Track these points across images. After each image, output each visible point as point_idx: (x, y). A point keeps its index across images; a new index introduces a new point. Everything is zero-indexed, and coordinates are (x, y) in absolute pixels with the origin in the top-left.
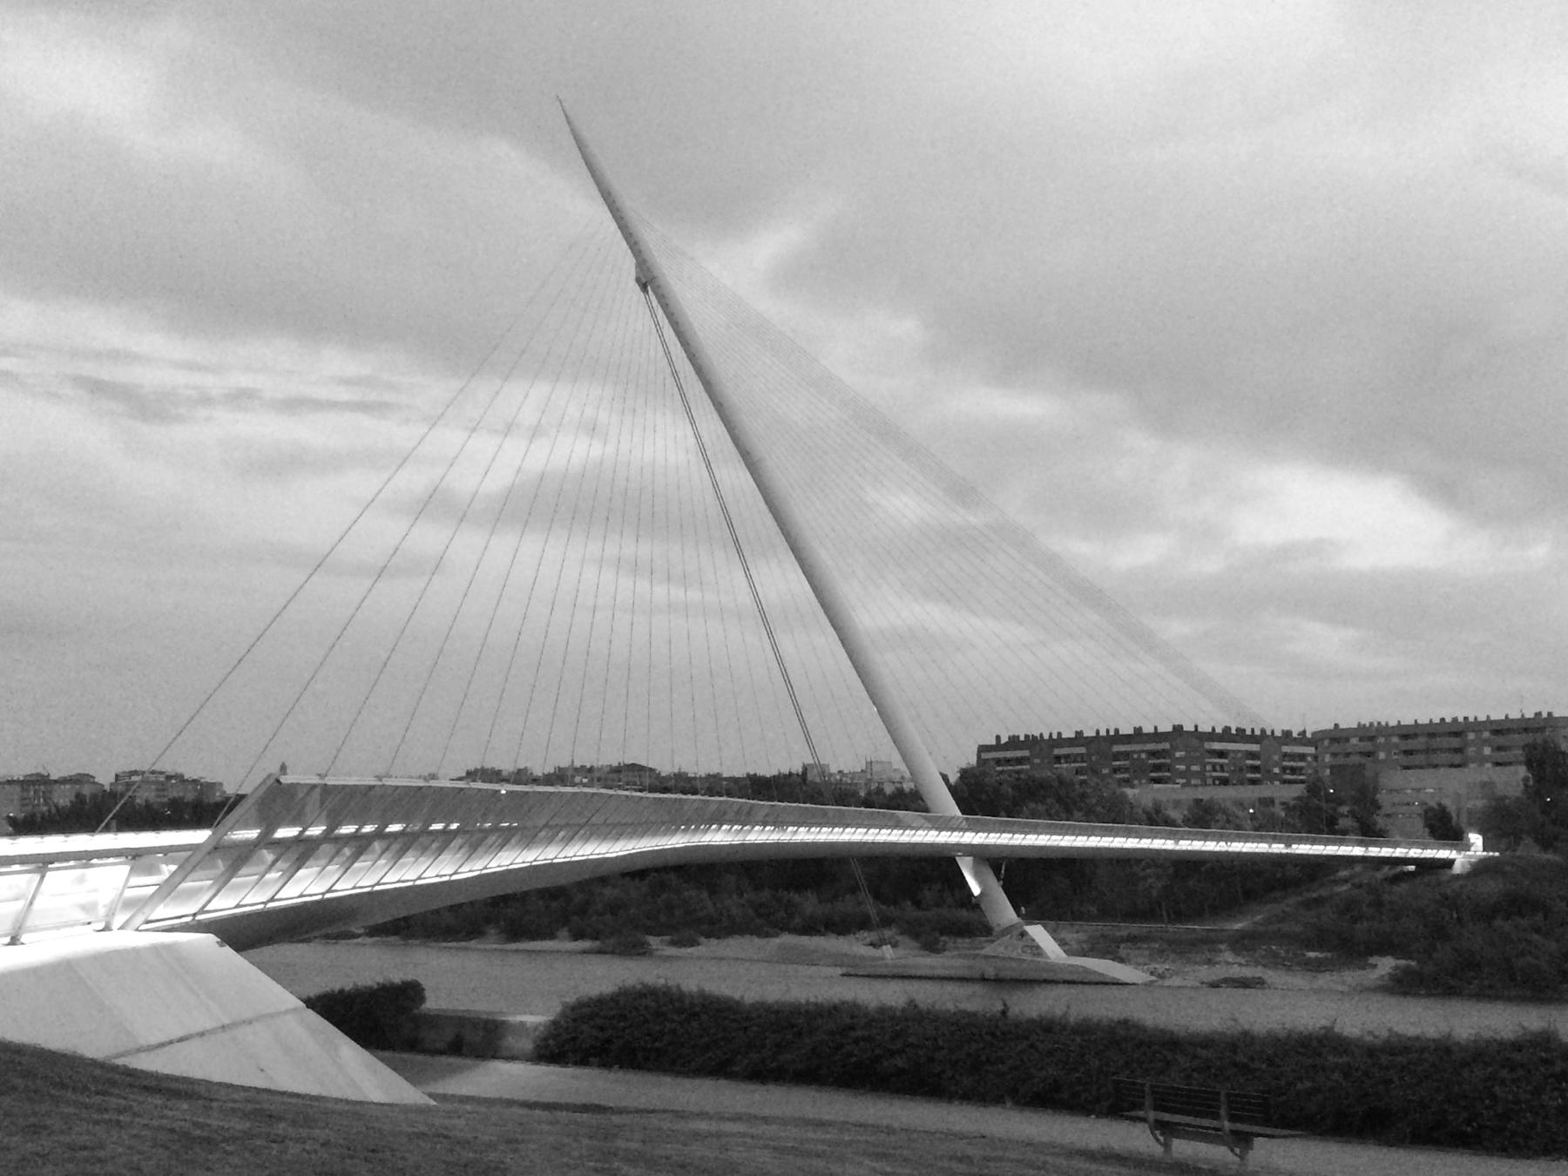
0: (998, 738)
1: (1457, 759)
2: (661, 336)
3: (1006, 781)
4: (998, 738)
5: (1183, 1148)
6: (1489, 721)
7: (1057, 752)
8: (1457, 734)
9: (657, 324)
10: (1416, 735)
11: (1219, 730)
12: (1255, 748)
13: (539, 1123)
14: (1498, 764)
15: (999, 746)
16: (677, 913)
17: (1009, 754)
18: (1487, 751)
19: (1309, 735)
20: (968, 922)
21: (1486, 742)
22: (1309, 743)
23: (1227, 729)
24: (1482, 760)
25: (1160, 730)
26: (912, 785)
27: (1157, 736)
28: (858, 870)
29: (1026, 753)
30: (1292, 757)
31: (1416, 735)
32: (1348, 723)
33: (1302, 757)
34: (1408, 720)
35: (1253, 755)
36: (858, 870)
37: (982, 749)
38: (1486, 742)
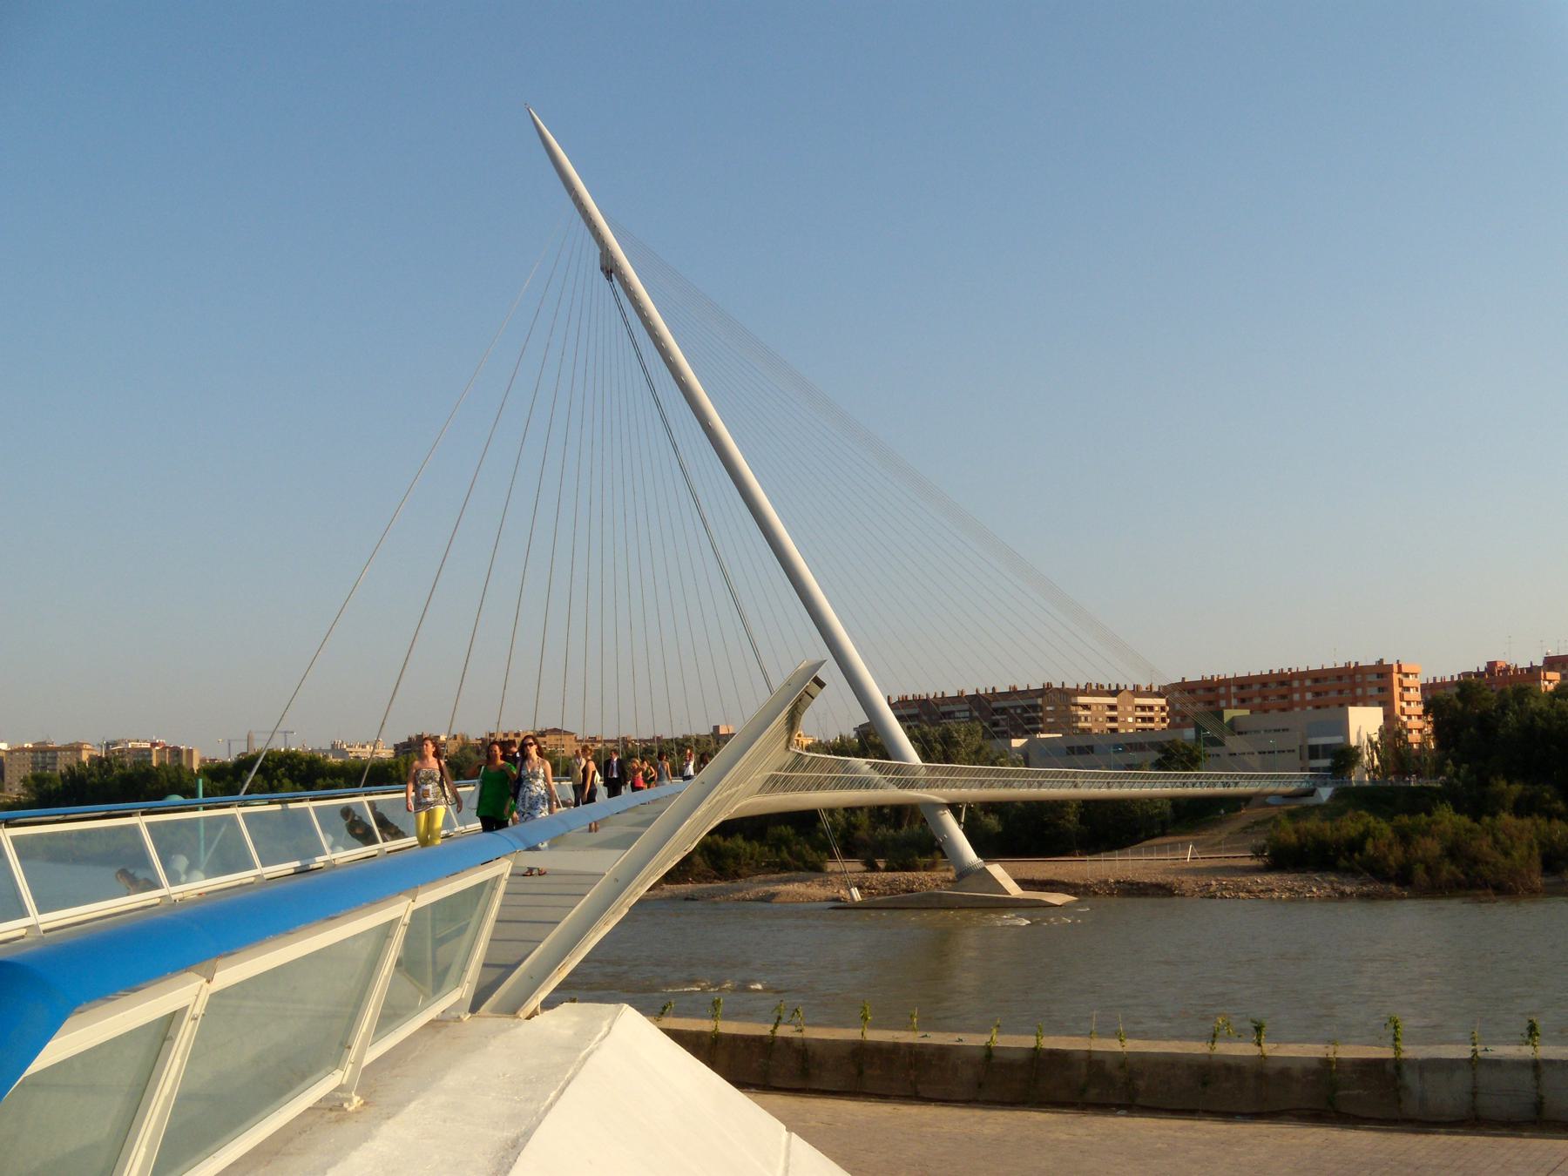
1: (1284, 703)
2: (624, 315)
3: (942, 725)
4: (716, 728)
5: (1029, 1042)
6: (1236, 679)
8: (1282, 683)
9: (621, 307)
10: (1326, 679)
11: (1082, 687)
12: (1112, 701)
14: (1318, 707)
18: (1309, 696)
20: (931, 847)
21: (1308, 689)
22: (1159, 695)
23: (1088, 685)
24: (1303, 704)
27: (1028, 693)
29: (916, 711)
30: (1143, 708)
31: (1326, 679)
32: (1193, 676)
33: (1151, 708)
34: (1242, 673)
35: (1112, 707)
37: (396, 747)
38: (1308, 689)
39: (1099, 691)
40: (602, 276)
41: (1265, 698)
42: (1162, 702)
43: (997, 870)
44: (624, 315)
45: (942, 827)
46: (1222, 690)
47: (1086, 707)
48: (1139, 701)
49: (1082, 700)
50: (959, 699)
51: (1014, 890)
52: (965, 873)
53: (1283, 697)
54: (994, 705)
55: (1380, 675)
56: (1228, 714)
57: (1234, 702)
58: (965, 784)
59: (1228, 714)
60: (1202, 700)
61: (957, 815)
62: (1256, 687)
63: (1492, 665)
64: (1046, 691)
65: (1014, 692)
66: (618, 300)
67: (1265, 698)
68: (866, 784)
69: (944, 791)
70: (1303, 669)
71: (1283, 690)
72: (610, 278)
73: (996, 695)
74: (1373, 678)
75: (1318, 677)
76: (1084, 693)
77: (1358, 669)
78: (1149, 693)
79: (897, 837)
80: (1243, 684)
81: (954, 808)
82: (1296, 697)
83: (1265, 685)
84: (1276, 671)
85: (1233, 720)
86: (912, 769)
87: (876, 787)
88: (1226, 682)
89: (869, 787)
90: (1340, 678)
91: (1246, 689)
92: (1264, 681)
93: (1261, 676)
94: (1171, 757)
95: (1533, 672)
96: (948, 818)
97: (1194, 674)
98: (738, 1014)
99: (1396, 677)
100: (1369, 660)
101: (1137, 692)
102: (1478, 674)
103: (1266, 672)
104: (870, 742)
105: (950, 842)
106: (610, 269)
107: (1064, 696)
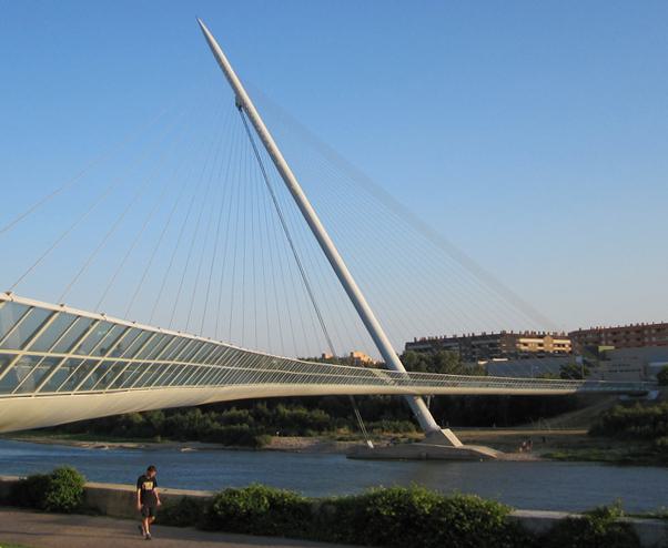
0: (324, 355)
1: (640, 343)
2: (248, 131)
3: (427, 356)
4: (324, 355)
6: (610, 329)
7: (473, 343)
9: (246, 126)
12: (541, 341)
13: (213, 421)
15: (416, 343)
16: (260, 427)
17: (421, 347)
19: (327, 357)
22: (567, 338)
24: (651, 343)
25: (476, 334)
26: (332, 355)
27: (493, 336)
28: (352, 399)
29: (430, 346)
30: (559, 345)
32: (586, 328)
36: (352, 399)
37: (408, 345)
38: (654, 335)
39: (533, 336)
40: (236, 109)
41: (628, 340)
42: (569, 342)
43: (447, 432)
44: (248, 131)
45: (418, 408)
47: (525, 344)
49: (522, 340)
50: (455, 339)
51: (458, 444)
52: (431, 433)
53: (639, 339)
54: (445, 345)
56: (601, 349)
59: (601, 349)
61: (425, 402)
63: (408, 345)
64: (503, 334)
65: (484, 337)
67: (628, 340)
68: (382, 382)
69: (420, 389)
70: (651, 323)
71: (639, 335)
73: (474, 338)
78: (563, 337)
79: (396, 409)
80: (615, 332)
82: (646, 340)
83: (628, 332)
85: (604, 351)
86: (400, 375)
88: (649, 328)
89: (384, 386)
90: (628, 332)
92: (627, 330)
93: (626, 327)
94: (568, 373)
96: (420, 402)
97: (586, 325)
101: (555, 337)
104: (386, 365)
106: (241, 105)
107: (514, 338)
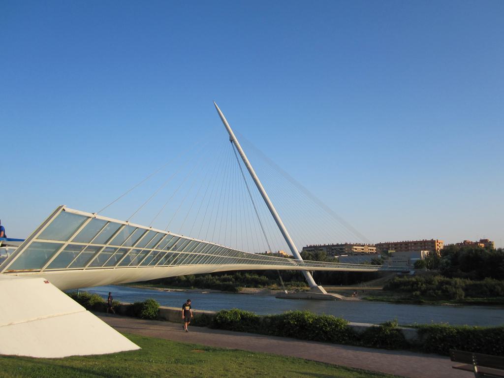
3: (312, 253)
12: (363, 248)
22: (374, 247)
24: (411, 250)
27: (342, 245)
29: (313, 249)
34: (415, 240)
37: (304, 248)
38: (413, 246)
40: (230, 142)
42: (375, 248)
43: (320, 287)
45: (308, 276)
46: (410, 245)
47: (356, 249)
48: (369, 248)
49: (354, 247)
50: (325, 246)
51: (325, 292)
52: (313, 288)
55: (432, 243)
56: (389, 252)
57: (393, 249)
58: (311, 266)
60: (383, 248)
61: (311, 273)
62: (399, 245)
63: (465, 241)
64: (346, 244)
65: (338, 245)
66: (234, 149)
67: (401, 248)
68: (292, 264)
69: (309, 268)
71: (407, 246)
72: (231, 142)
73: (333, 246)
74: (430, 244)
75: (416, 243)
76: (355, 245)
77: (426, 242)
79: (299, 276)
80: (396, 244)
81: (310, 272)
82: (410, 248)
84: (404, 241)
85: (391, 253)
86: (300, 261)
87: (294, 265)
89: (292, 266)
90: (421, 244)
91: (396, 246)
92: (401, 244)
94: (374, 262)
95: (476, 243)
96: (309, 273)
98: (125, 333)
99: (436, 244)
100: (429, 239)
101: (369, 246)
102: (461, 244)
103: (422, 240)
104: (294, 257)
105: (309, 280)
106: (232, 140)
107: (351, 246)
